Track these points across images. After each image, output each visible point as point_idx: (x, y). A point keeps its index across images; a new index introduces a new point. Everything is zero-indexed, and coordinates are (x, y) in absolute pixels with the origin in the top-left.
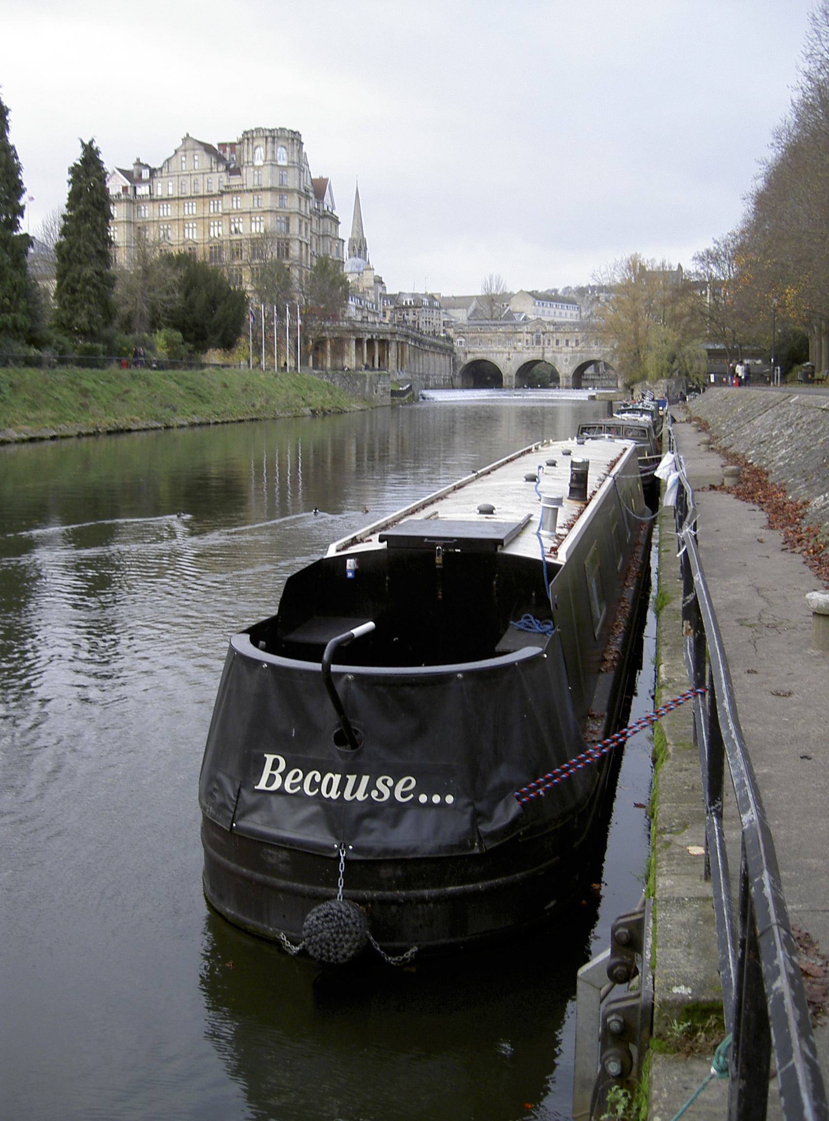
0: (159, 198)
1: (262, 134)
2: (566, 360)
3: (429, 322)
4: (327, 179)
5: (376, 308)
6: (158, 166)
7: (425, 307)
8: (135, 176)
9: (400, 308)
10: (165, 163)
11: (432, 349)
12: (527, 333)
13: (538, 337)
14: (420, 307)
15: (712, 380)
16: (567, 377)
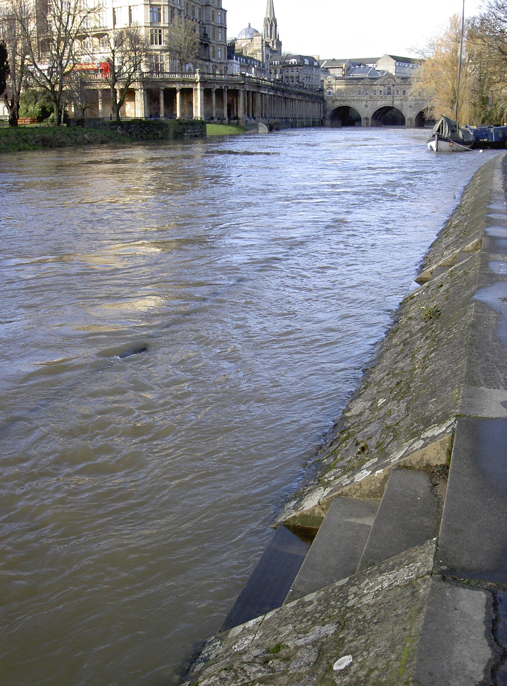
2: (410, 106)
3: (310, 77)
5: (263, 67)
7: (306, 65)
9: (287, 66)
11: (300, 97)
12: (381, 85)
13: (389, 89)
14: (302, 66)
16: (410, 119)
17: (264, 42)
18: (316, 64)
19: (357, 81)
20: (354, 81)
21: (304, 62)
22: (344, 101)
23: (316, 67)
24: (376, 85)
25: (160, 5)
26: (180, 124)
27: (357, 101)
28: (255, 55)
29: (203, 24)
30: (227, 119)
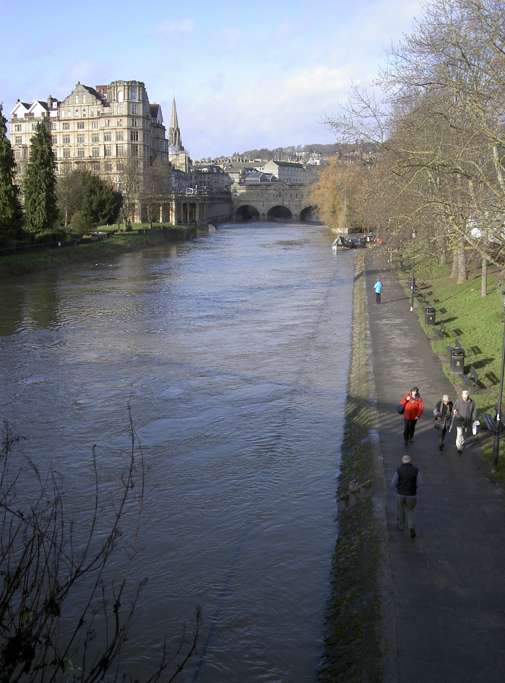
0: (63, 119)
1: (122, 84)
2: (296, 206)
4: (159, 105)
5: (187, 176)
6: (62, 101)
7: (215, 173)
8: (49, 106)
10: (66, 98)
12: (274, 190)
13: (280, 193)
14: (212, 174)
15: (60, 245)
16: (296, 215)
17: (187, 158)
18: (221, 172)
19: (256, 187)
20: (254, 187)
21: (213, 170)
22: (246, 202)
23: (222, 174)
24: (270, 190)
25: (138, 144)
26: (189, 231)
27: (256, 202)
28: (181, 168)
29: (155, 151)
30: (189, 222)
